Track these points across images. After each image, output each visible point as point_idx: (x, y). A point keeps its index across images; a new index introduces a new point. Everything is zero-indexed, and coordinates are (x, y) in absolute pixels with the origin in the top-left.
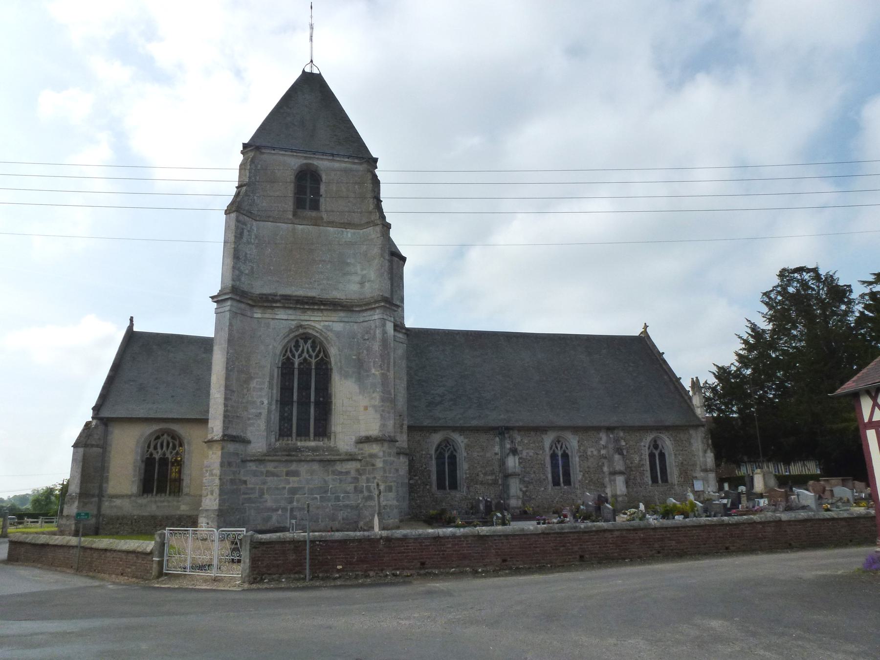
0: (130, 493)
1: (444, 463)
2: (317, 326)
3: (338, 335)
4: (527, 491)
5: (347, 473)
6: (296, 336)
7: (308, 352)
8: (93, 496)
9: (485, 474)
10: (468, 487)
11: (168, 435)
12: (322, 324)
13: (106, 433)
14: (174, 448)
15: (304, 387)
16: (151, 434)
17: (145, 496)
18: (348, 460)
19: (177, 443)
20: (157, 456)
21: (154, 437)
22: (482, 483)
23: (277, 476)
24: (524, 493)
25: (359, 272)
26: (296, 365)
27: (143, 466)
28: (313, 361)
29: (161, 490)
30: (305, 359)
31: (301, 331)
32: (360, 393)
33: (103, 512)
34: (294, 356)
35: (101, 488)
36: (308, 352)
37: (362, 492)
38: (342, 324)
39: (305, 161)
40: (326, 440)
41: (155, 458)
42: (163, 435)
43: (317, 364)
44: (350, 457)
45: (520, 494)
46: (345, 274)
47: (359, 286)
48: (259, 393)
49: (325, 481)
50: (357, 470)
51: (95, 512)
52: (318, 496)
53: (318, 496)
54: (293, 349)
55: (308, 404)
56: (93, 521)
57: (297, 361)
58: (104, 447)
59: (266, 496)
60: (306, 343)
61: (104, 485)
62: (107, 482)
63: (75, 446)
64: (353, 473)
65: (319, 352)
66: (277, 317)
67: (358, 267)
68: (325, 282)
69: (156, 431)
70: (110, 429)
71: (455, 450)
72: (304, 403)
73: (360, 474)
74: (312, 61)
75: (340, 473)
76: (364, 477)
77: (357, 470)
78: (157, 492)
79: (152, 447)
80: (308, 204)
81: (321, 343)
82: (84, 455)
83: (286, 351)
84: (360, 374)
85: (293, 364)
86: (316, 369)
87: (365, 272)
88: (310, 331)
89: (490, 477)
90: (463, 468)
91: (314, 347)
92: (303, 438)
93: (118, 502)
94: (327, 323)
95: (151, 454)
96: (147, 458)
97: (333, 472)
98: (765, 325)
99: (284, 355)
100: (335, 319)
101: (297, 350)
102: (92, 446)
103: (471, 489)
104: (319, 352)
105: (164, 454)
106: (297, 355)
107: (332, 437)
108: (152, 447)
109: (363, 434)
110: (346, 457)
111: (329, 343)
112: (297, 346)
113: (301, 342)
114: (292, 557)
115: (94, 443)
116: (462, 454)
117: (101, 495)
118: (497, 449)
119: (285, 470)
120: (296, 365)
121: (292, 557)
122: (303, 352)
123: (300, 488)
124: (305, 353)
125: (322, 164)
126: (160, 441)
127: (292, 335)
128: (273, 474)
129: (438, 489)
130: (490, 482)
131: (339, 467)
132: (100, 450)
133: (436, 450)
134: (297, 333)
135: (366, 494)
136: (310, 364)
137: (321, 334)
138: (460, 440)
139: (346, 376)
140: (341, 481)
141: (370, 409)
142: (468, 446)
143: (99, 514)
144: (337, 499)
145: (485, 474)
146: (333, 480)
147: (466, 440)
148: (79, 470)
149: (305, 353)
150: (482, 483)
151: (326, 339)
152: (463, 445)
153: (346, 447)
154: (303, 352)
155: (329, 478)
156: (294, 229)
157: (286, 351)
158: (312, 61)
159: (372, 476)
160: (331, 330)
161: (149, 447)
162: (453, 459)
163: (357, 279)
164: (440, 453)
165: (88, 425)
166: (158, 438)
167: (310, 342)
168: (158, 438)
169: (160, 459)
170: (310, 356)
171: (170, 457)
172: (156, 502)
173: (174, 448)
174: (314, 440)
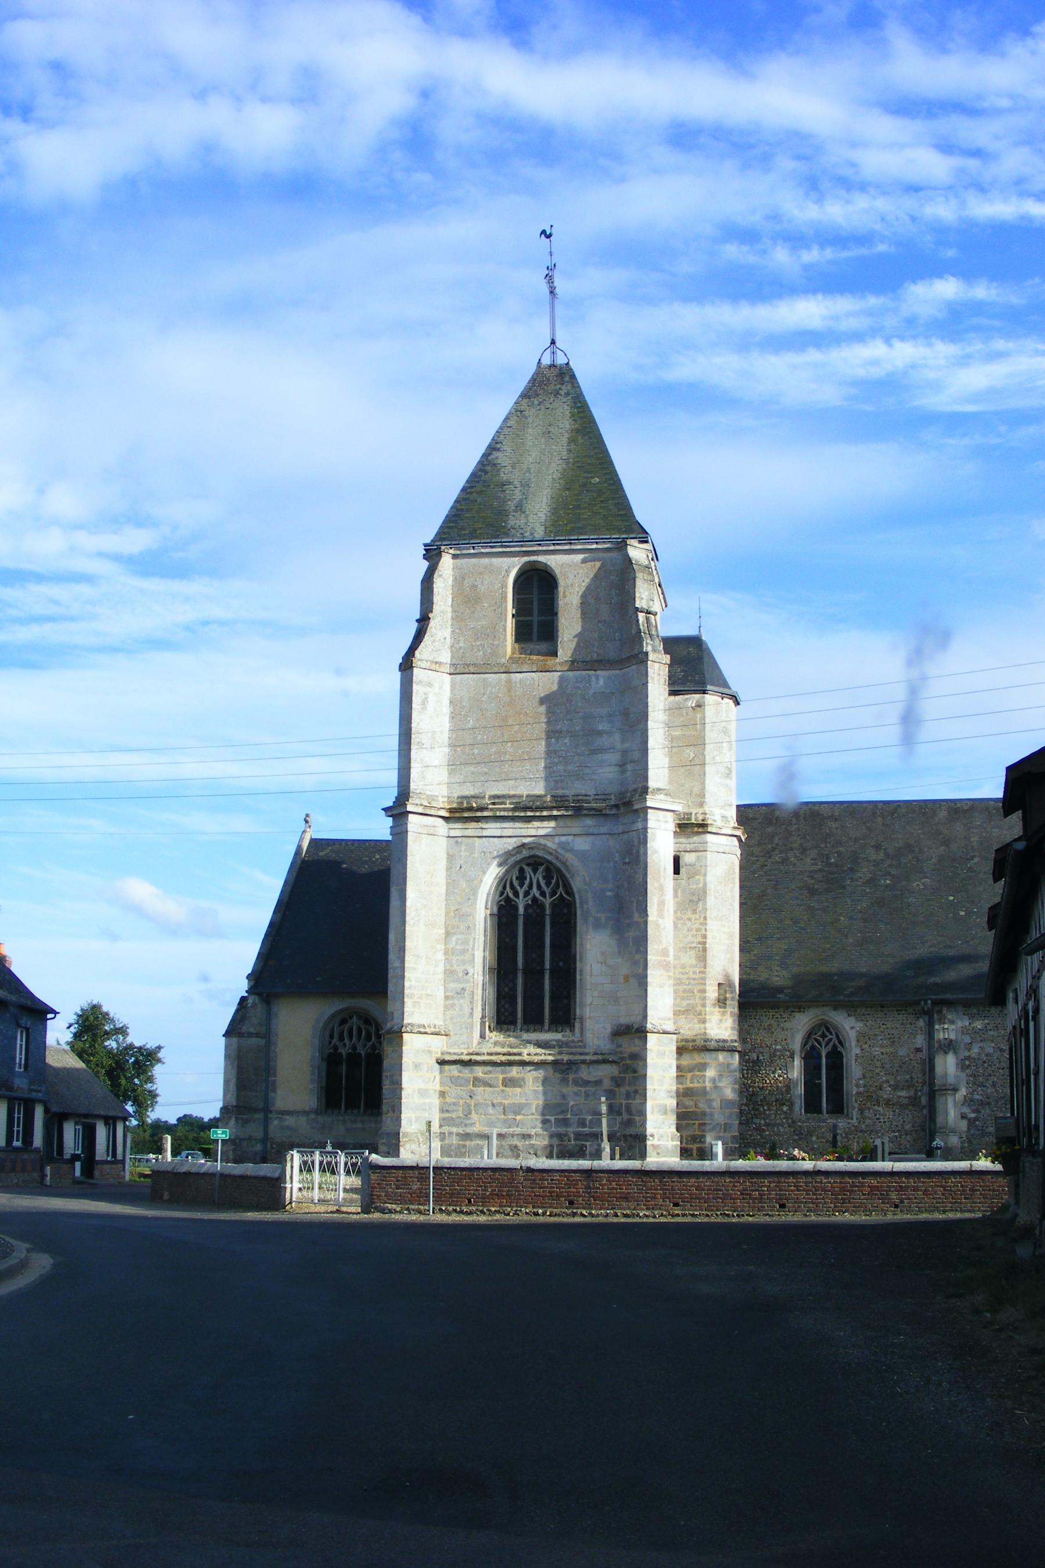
0: (307, 1108)
1: (819, 1067)
2: (549, 844)
3: (582, 856)
4: (976, 1119)
5: (598, 1083)
6: (517, 862)
7: (539, 886)
8: (256, 1110)
9: (896, 1087)
10: (861, 1111)
11: (359, 1017)
12: (557, 840)
13: (269, 1016)
14: (369, 1037)
15: (534, 944)
16: (333, 1017)
17: (330, 1111)
18: (597, 1062)
19: (373, 1030)
20: (343, 1051)
21: (338, 1019)
22: (888, 1103)
23: (490, 1086)
24: (971, 1123)
25: (618, 746)
26: (521, 910)
27: (324, 1066)
28: (548, 902)
29: (352, 1104)
30: (535, 899)
31: (525, 853)
32: (619, 953)
33: (271, 1134)
34: (516, 894)
35: (266, 1100)
36: (539, 886)
37: (619, 1113)
38: (589, 839)
39: (526, 559)
40: (568, 1033)
41: (341, 1054)
42: (351, 1017)
43: (553, 905)
44: (600, 1057)
45: (963, 1125)
46: (593, 752)
47: (617, 769)
48: (460, 958)
49: (564, 1097)
50: (613, 1079)
51: (260, 1135)
52: (552, 1118)
53: (552, 1118)
54: (516, 883)
55: (541, 972)
56: (259, 1147)
57: (521, 905)
58: (267, 1035)
59: (474, 1116)
60: (535, 871)
61: (271, 1095)
62: (274, 1090)
63: (228, 1034)
64: (607, 1084)
65: (557, 886)
66: (485, 833)
67: (617, 737)
68: (561, 767)
69: (347, 1009)
70: (275, 1008)
71: (840, 1042)
72: (533, 973)
73: (618, 1086)
74: (553, 342)
75: (586, 1083)
76: (623, 1090)
77: (613, 1079)
78: (346, 1108)
79: (336, 1035)
80: (535, 630)
81: (559, 871)
82: (240, 1049)
83: (504, 888)
84: (618, 920)
85: (516, 908)
86: (553, 915)
87: (626, 745)
88: (540, 853)
89: (903, 1094)
90: (854, 1072)
91: (548, 878)
92: (532, 1027)
93: (290, 1121)
94: (563, 839)
95: (336, 1048)
96: (330, 1055)
97: (576, 1082)
98: (149, 1086)
99: (502, 894)
100: (574, 831)
101: (521, 885)
102: (250, 1035)
103: (867, 1113)
104: (557, 886)
105: (354, 1048)
106: (521, 896)
107: (577, 1025)
108: (336, 1035)
109: (624, 1020)
110: (595, 1058)
111: (569, 872)
112: (521, 878)
113: (528, 870)
114: (416, 1186)
115: (252, 1030)
116: (853, 1051)
117: (267, 1110)
118: (920, 1041)
119: (501, 1077)
120: (521, 910)
121: (416, 1186)
122: (531, 886)
123: (526, 1105)
124: (535, 889)
125: (555, 562)
126: (346, 1027)
127: (512, 860)
128: (487, 1084)
129: (808, 1110)
130: (905, 1101)
131: (584, 1073)
132: (261, 1042)
133: (804, 1044)
134: (519, 857)
135: (625, 1116)
136: (542, 907)
137: (557, 858)
138: (849, 1026)
139: (597, 926)
140: (587, 1095)
141: (632, 980)
142: (861, 1036)
143: (265, 1139)
144: (582, 1123)
145: (896, 1087)
146: (576, 1094)
147: (859, 1025)
148: (234, 1071)
149: (535, 889)
150: (888, 1103)
151: (564, 864)
152: (852, 1034)
153: (596, 1042)
154: (531, 886)
155: (569, 1090)
156: (509, 681)
157: (504, 888)
158: (553, 342)
159: (633, 1088)
160: (571, 851)
161: (331, 1037)
162: (836, 1061)
163: (613, 757)
164: (813, 1047)
165: (243, 999)
166: (343, 1022)
167: (541, 869)
168: (343, 1022)
169: (349, 1055)
170: (543, 894)
171: (363, 1053)
172: (344, 1122)
173: (369, 1037)
174: (549, 1030)
